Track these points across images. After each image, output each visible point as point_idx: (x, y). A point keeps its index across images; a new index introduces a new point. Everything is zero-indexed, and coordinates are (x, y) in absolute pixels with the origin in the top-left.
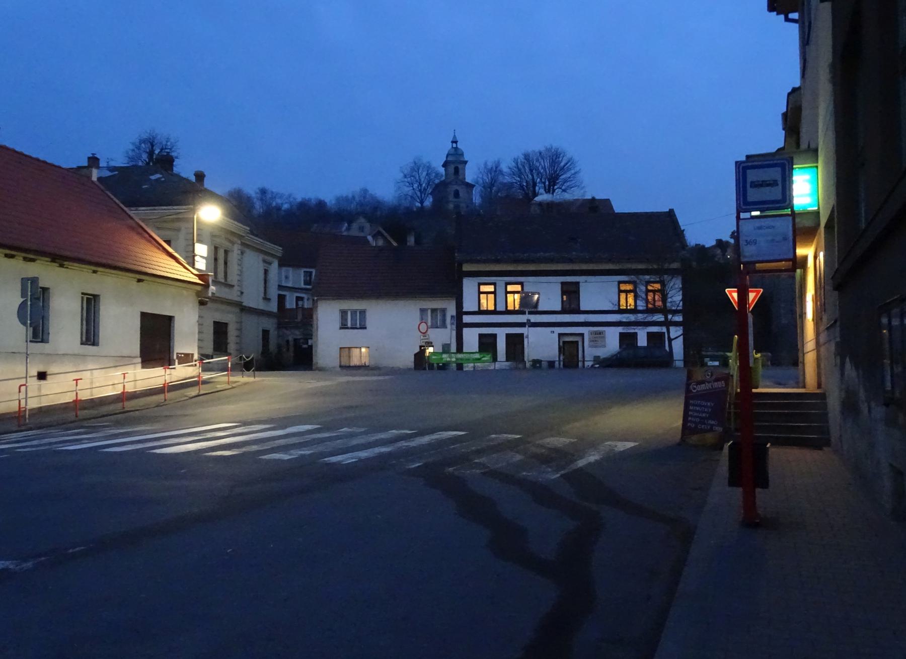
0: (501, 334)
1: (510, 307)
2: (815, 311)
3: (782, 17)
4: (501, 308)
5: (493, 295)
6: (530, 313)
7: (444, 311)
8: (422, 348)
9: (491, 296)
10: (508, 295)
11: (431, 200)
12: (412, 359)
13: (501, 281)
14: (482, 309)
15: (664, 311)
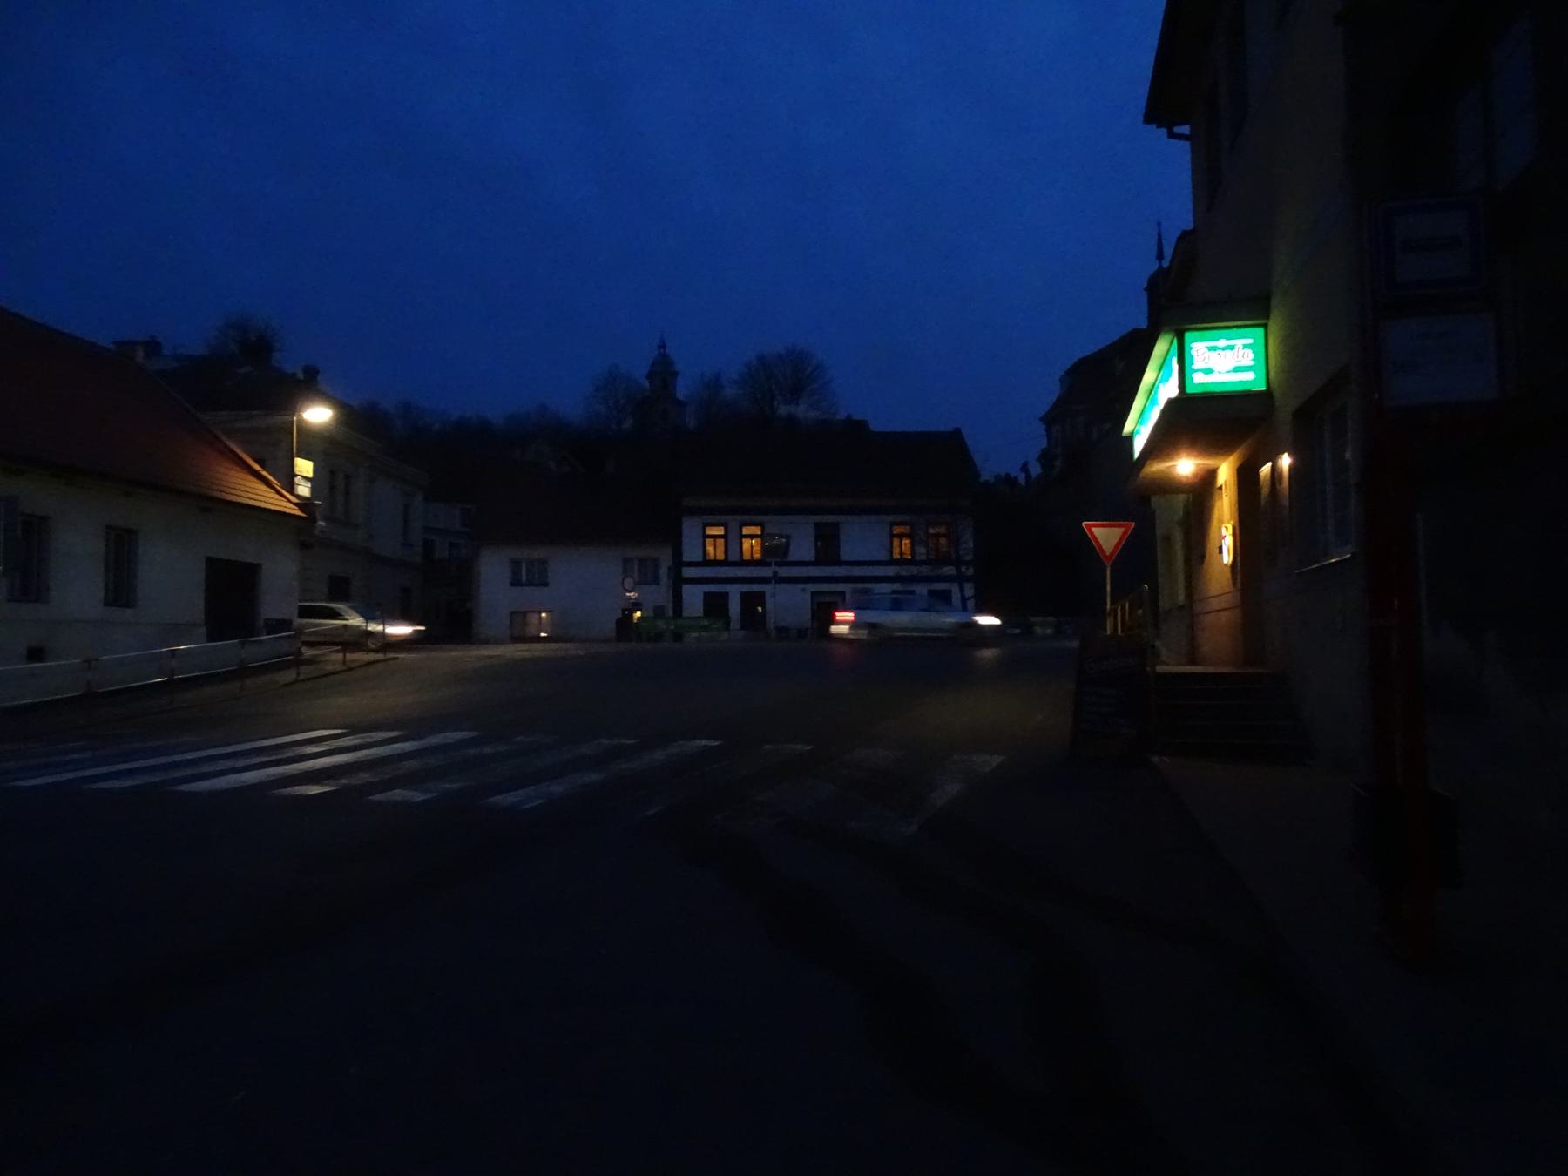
0: (735, 592)
1: (747, 556)
2: (1238, 548)
3: (1164, 130)
4: (734, 557)
5: (723, 540)
6: (777, 564)
7: (656, 564)
8: (627, 612)
9: (721, 542)
10: (744, 540)
11: (631, 421)
12: (613, 626)
13: (733, 520)
14: (708, 558)
15: (958, 563)
